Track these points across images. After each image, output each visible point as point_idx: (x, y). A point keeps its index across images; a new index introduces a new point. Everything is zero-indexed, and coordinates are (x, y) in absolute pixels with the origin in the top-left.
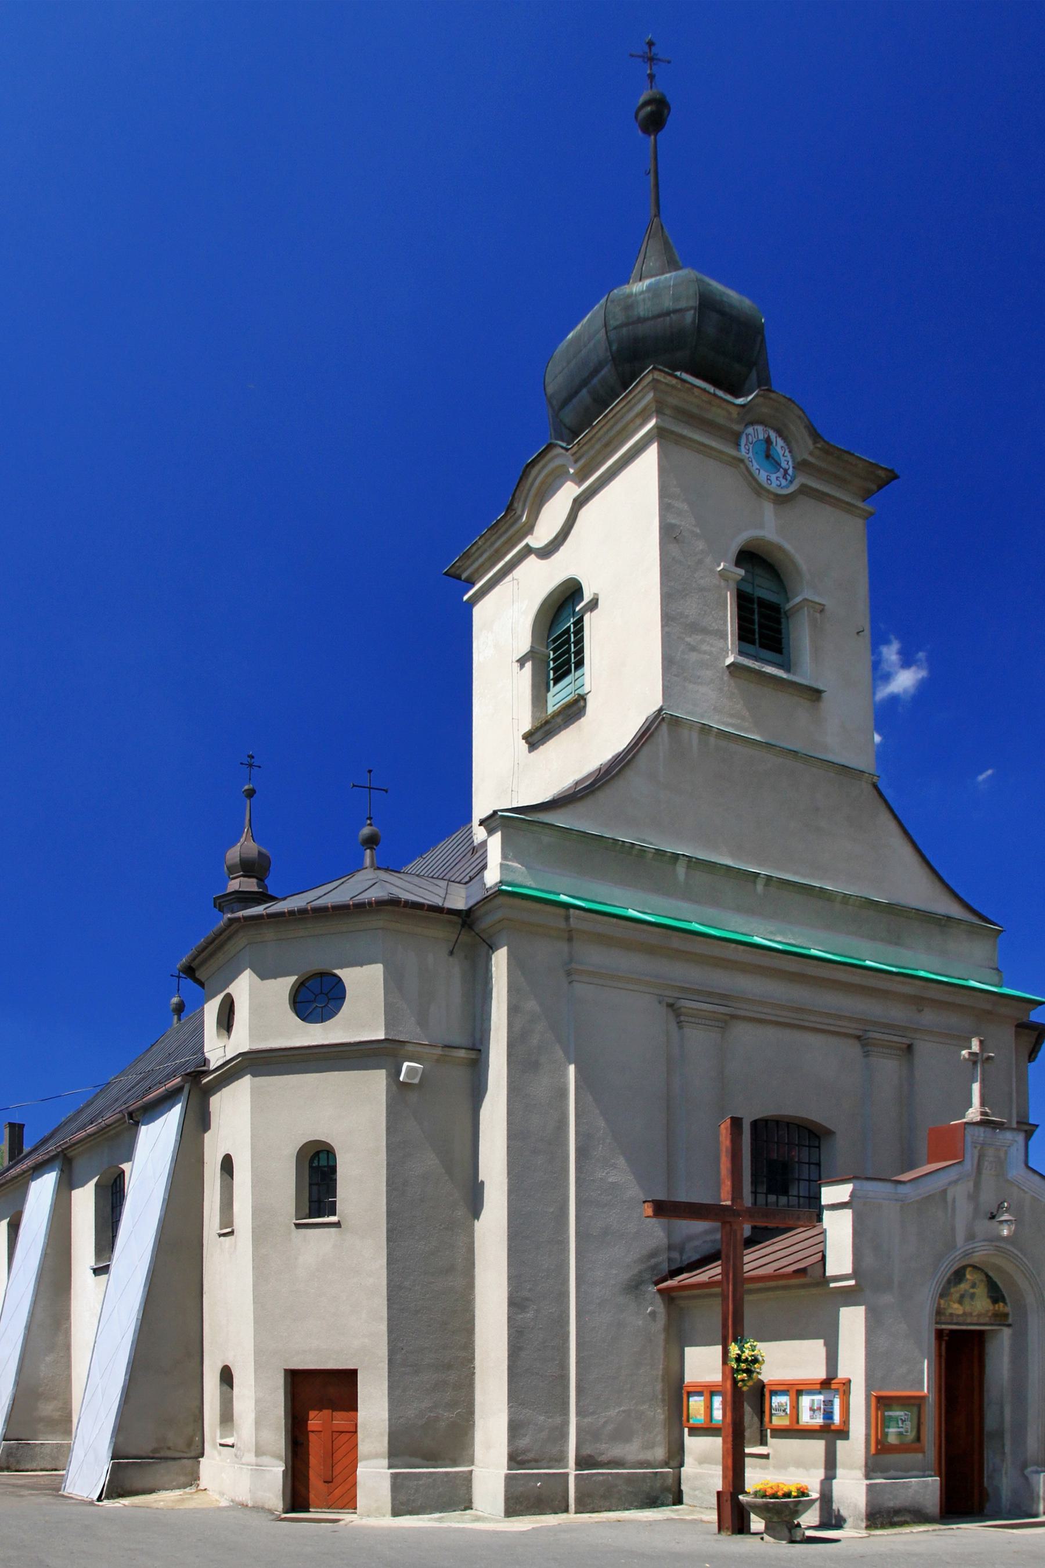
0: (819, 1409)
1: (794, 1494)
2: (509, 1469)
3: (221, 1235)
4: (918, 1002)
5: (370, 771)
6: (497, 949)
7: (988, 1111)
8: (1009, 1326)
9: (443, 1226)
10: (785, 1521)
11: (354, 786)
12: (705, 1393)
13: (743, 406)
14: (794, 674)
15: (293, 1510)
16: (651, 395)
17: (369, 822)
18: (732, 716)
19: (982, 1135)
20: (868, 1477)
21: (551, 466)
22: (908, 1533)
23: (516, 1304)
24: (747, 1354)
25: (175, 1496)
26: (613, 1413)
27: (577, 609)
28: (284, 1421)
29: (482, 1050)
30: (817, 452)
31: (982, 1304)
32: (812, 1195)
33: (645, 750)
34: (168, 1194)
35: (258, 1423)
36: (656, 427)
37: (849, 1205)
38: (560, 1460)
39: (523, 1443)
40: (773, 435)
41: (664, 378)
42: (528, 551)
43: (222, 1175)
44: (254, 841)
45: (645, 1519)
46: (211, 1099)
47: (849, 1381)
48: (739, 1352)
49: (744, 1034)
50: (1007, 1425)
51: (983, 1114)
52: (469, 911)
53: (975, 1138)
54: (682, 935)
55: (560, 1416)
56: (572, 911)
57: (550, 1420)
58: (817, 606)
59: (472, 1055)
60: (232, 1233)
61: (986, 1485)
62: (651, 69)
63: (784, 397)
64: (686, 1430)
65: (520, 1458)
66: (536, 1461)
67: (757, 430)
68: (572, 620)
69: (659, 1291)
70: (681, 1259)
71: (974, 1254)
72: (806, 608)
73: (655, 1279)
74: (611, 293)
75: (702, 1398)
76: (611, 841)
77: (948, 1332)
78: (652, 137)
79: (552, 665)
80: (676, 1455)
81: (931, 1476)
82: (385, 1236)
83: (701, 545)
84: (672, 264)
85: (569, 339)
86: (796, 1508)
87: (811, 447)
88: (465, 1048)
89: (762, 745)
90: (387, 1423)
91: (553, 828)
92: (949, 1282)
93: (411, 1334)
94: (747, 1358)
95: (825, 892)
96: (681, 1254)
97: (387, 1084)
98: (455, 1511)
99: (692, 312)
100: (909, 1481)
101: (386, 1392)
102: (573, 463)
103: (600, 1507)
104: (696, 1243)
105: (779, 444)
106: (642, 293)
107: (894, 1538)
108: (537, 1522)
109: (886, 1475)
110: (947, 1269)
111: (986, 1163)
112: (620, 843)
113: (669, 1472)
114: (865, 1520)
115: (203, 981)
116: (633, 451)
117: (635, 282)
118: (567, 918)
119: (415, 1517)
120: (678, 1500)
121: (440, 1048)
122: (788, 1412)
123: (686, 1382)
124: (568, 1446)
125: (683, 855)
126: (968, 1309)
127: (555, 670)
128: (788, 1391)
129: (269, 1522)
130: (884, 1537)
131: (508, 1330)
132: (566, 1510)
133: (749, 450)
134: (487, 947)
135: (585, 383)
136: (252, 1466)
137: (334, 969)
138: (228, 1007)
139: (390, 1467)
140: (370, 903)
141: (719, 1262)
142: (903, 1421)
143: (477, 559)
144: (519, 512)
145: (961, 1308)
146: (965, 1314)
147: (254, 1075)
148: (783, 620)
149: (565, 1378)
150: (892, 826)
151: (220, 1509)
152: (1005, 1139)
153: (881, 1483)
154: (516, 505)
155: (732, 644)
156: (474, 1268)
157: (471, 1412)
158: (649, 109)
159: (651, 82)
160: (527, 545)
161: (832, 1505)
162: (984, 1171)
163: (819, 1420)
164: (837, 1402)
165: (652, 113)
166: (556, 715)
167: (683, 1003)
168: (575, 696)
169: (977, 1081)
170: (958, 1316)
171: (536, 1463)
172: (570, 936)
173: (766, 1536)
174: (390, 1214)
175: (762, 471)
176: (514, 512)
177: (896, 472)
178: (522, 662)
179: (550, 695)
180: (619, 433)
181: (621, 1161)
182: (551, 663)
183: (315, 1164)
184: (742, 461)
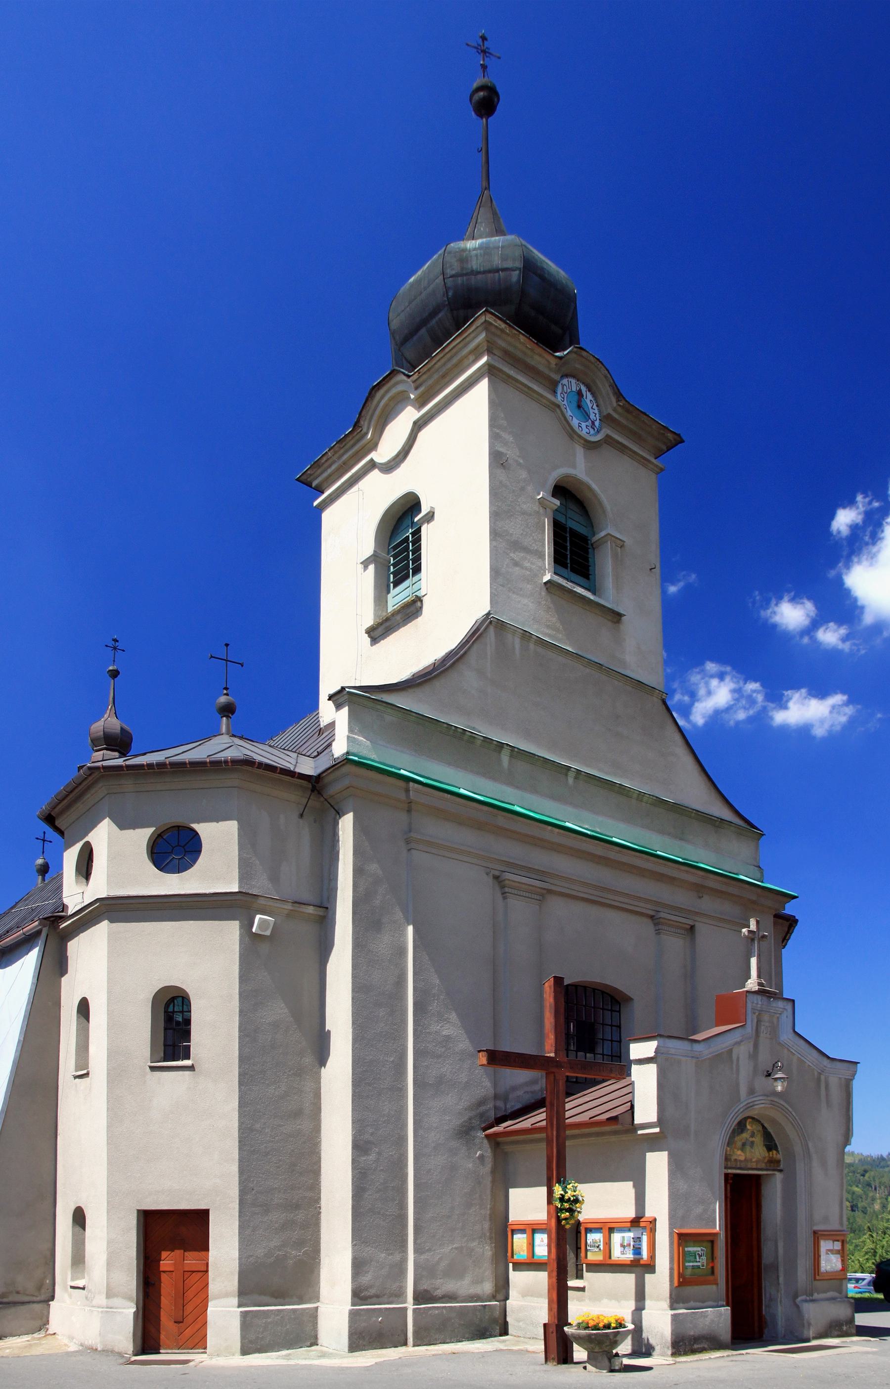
0: (629, 1245)
1: (613, 1325)
2: (353, 1304)
3: (76, 1077)
4: (700, 890)
5: (227, 645)
6: (344, 815)
8: (781, 1171)
10: (606, 1351)
11: (212, 657)
12: (527, 1231)
13: (560, 358)
14: (600, 597)
15: (144, 1352)
16: (483, 335)
17: (225, 692)
18: (548, 627)
19: (760, 1003)
20: (672, 1308)
21: (394, 391)
23: (360, 1147)
24: (569, 1194)
25: (23, 1342)
26: (447, 1249)
27: (416, 520)
29: (329, 907)
30: (620, 410)
31: (759, 1152)
32: (614, 1054)
33: (475, 647)
34: (23, 1036)
35: (110, 1265)
36: (487, 364)
37: (654, 1060)
38: (399, 1295)
39: (366, 1279)
40: (584, 389)
41: (495, 320)
42: (372, 465)
43: (78, 1018)
44: (117, 718)
45: (477, 1351)
46: (69, 944)
47: (655, 1220)
48: (562, 1193)
49: (558, 908)
50: (781, 1259)
51: (760, 984)
52: (319, 778)
55: (399, 1253)
56: (411, 784)
57: (390, 1257)
59: (320, 912)
60: (87, 1075)
61: (764, 1313)
62: (484, 60)
63: (594, 357)
64: (511, 1265)
66: (377, 1296)
68: (410, 531)
69: (487, 1136)
70: (506, 1107)
71: (756, 1107)
72: (609, 542)
73: (483, 1125)
74: (448, 246)
75: (525, 1236)
76: (445, 725)
77: (732, 1176)
78: (484, 119)
79: (392, 569)
80: (502, 1289)
81: (723, 1306)
82: (237, 1080)
83: (524, 474)
84: (499, 232)
85: (410, 283)
86: (615, 1339)
87: (615, 404)
88: (314, 906)
89: (573, 656)
90: (238, 1261)
91: (394, 707)
92: (734, 1131)
93: (261, 1175)
94: (569, 1198)
95: (624, 789)
96: (505, 1104)
97: (240, 934)
99: (517, 272)
100: (706, 1311)
101: (237, 1231)
102: (413, 390)
103: (436, 1339)
104: (520, 1093)
105: (588, 397)
106: (475, 249)
107: (695, 1365)
108: (379, 1356)
109: (686, 1305)
110: (731, 1122)
111: (763, 1027)
112: (453, 728)
114: (670, 1348)
115: (63, 830)
116: (467, 384)
117: (468, 240)
118: (407, 791)
119: (263, 1355)
120: (504, 1332)
121: (290, 904)
122: (602, 1249)
123: (510, 1221)
124: (407, 1282)
126: (748, 1155)
127: (395, 574)
128: (601, 1229)
129: (119, 1366)
130: (688, 1364)
132: (405, 1343)
133: (564, 398)
134: (334, 812)
135: (424, 322)
136: (103, 1308)
137: (192, 823)
138: (87, 856)
139: (239, 1306)
140: (226, 762)
141: (544, 1109)
142: (700, 1256)
143: (326, 470)
144: (365, 430)
145: (742, 1154)
146: (746, 1160)
147: (112, 921)
148: (590, 550)
149: (403, 1217)
151: (69, 1354)
153: (683, 1313)
154: (362, 422)
155: (549, 564)
156: (320, 1112)
157: (316, 1250)
158: (481, 94)
159: (484, 72)
160: (372, 460)
161: (642, 1335)
162: (762, 1035)
163: (629, 1256)
164: (645, 1239)
165: (484, 98)
166: (395, 613)
167: (508, 876)
168: (413, 597)
169: (755, 956)
170: (740, 1161)
171: (377, 1298)
172: (409, 807)
173: (589, 1367)
174: (242, 1059)
175: (574, 418)
176: (361, 429)
178: (365, 564)
179: (390, 596)
180: (456, 365)
181: (453, 1016)
182: (392, 567)
183: (171, 1009)
184: (559, 406)
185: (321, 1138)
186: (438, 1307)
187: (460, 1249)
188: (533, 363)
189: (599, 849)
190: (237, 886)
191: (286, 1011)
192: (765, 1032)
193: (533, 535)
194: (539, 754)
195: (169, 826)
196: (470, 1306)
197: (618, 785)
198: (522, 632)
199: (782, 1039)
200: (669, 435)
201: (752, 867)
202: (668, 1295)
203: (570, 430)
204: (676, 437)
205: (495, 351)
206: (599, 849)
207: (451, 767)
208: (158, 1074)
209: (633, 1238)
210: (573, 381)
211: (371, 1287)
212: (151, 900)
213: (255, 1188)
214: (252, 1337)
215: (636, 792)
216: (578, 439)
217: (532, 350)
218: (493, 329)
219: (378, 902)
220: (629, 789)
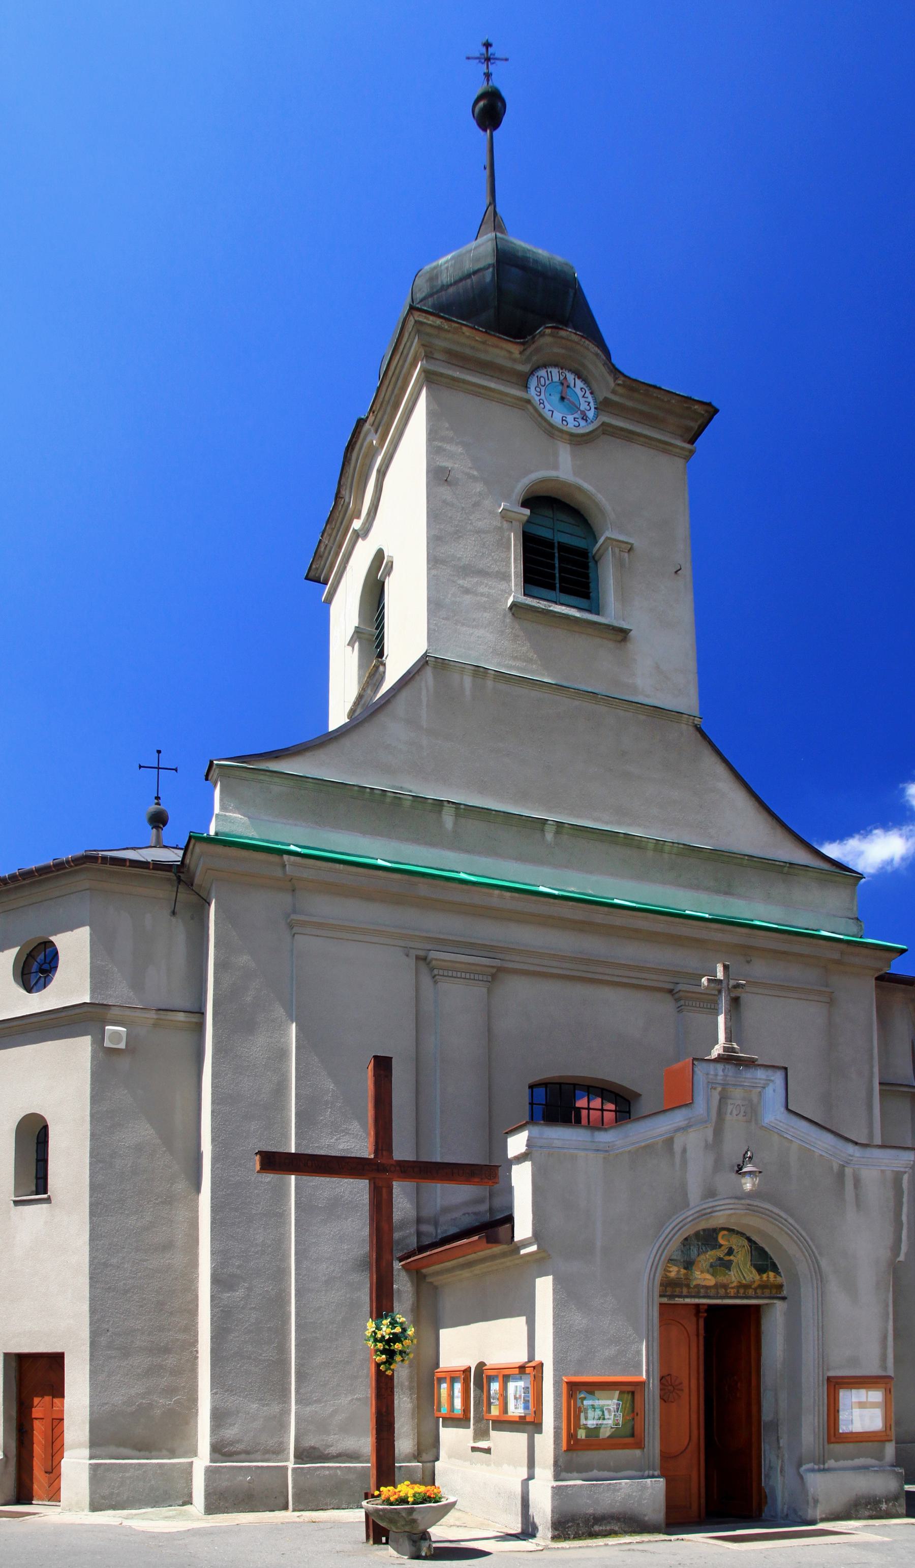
0: (520, 1396)
1: (411, 1499)
2: (212, 1461)
5: (159, 752)
7: (736, 1046)
9: (160, 1200)
11: (140, 767)
14: (603, 616)
18: (515, 658)
20: (557, 1478)
22: (600, 1546)
26: (344, 1400)
28: (2, 1407)
30: (620, 390)
38: (278, 1451)
39: (230, 1433)
40: (570, 377)
41: (426, 318)
53: (711, 1077)
54: (430, 881)
55: (279, 1403)
56: (286, 857)
58: (624, 546)
61: (763, 1485)
66: (247, 1453)
67: (551, 372)
77: (706, 1307)
83: (479, 487)
86: (410, 1517)
87: (612, 384)
90: (88, 1409)
91: (281, 775)
93: (119, 1315)
94: (383, 1337)
97: (92, 1049)
98: (171, 1506)
99: (491, 270)
101: (88, 1376)
103: (326, 1504)
109: (585, 1475)
111: (730, 1108)
112: (368, 790)
113: (418, 1466)
121: (154, 1012)
125: (448, 801)
131: (212, 1310)
132: (286, 1508)
133: (540, 392)
137: (52, 935)
139: (91, 1458)
144: (347, 500)
148: (591, 564)
149: (285, 1362)
150: (720, 769)
152: (756, 1079)
154: (343, 492)
155: (516, 585)
158: (481, 104)
161: (528, 1511)
162: (728, 1117)
167: (433, 955)
171: (248, 1454)
172: (292, 886)
174: (94, 1187)
176: (343, 500)
177: (715, 404)
184: (528, 402)
185: (198, 1274)
186: (328, 1467)
188: (488, 358)
189: (660, 925)
190: (89, 997)
191: (152, 1131)
192: (735, 1112)
193: (493, 554)
194: (497, 809)
195: (36, 944)
197: (622, 835)
198: (473, 668)
199: (766, 1120)
200: (696, 407)
201: (844, 920)
202: (552, 1462)
203: (547, 427)
204: (706, 407)
205: (436, 355)
206: (660, 925)
208: (20, 1208)
209: (523, 1388)
210: (555, 371)
211: (238, 1442)
213: (111, 1329)
215: (650, 841)
216: (560, 434)
217: (484, 343)
218: (429, 330)
219: (249, 999)
220: (639, 838)
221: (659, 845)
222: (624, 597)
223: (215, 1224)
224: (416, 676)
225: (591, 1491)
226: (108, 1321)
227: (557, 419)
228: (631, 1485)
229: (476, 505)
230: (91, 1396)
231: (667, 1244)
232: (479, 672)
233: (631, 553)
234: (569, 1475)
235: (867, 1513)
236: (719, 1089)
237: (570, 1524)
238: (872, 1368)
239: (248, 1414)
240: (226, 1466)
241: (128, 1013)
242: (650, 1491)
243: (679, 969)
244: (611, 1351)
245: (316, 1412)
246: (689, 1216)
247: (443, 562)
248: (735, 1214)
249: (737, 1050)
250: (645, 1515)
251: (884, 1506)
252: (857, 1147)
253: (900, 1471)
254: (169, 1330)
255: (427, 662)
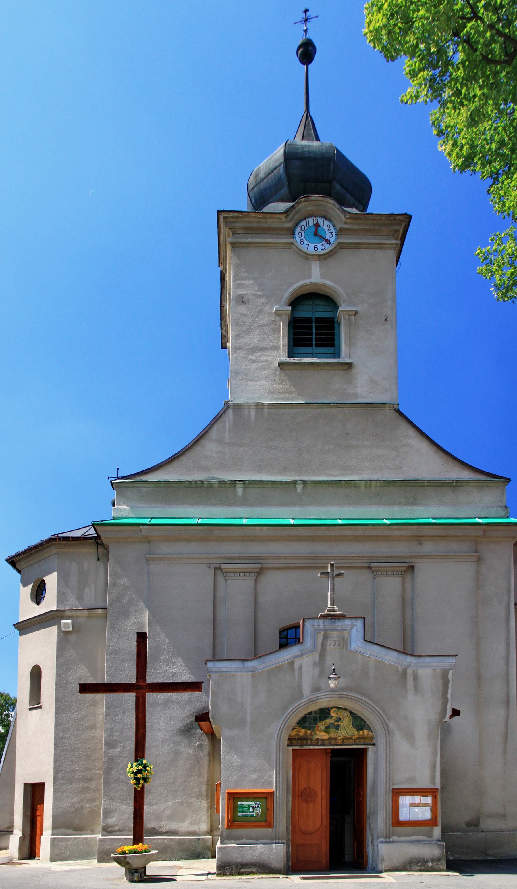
5: (118, 469)
9: (89, 704)
18: (281, 393)
26: (170, 803)
30: (349, 221)
41: (228, 214)
53: (315, 627)
56: (141, 527)
58: (351, 313)
65: (109, 830)
66: (120, 831)
71: (319, 700)
87: (344, 219)
89: (303, 406)
109: (238, 842)
125: (239, 481)
139: (53, 835)
142: (253, 808)
150: (411, 432)
152: (345, 625)
155: (283, 352)
172: (148, 540)
181: (179, 660)
187: (181, 804)
191: (86, 670)
192: (332, 645)
196: (187, 838)
197: (344, 482)
199: (352, 647)
200: (398, 217)
207: (194, 506)
211: (115, 825)
212: (26, 623)
213: (64, 770)
214: (58, 852)
220: (354, 482)
221: (368, 484)
222: (351, 343)
223: (107, 715)
224: (223, 415)
225: (240, 850)
226: (63, 766)
227: (311, 249)
228: (263, 847)
229: (260, 311)
230: (53, 804)
231: (289, 718)
232: (259, 405)
233: (357, 315)
234: (229, 842)
235: (418, 868)
236: (323, 633)
237: (227, 868)
238: (424, 783)
239: (121, 811)
240: (108, 838)
241: (74, 612)
242: (275, 851)
243: (372, 555)
244: (255, 776)
245: (155, 809)
246: (302, 703)
247: (240, 348)
248: (331, 700)
249: (336, 610)
250: (272, 864)
251: (430, 864)
252: (413, 658)
253: (443, 844)
254: (93, 769)
255: (229, 406)
